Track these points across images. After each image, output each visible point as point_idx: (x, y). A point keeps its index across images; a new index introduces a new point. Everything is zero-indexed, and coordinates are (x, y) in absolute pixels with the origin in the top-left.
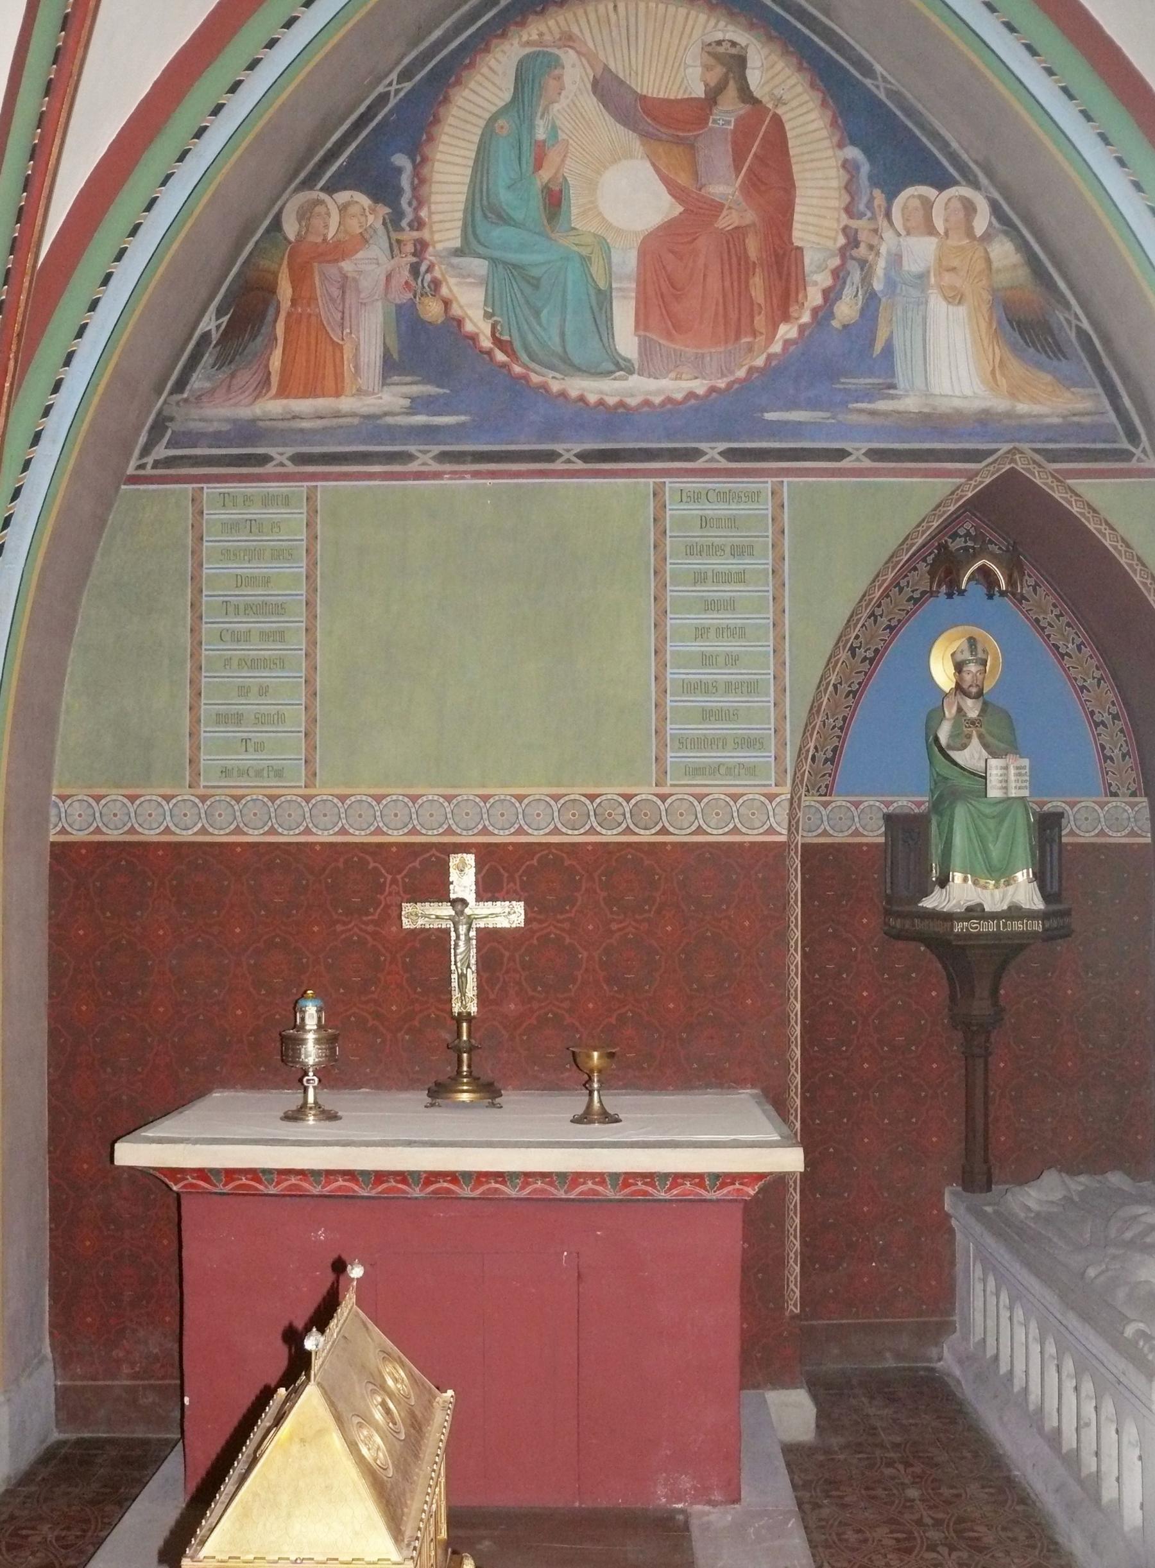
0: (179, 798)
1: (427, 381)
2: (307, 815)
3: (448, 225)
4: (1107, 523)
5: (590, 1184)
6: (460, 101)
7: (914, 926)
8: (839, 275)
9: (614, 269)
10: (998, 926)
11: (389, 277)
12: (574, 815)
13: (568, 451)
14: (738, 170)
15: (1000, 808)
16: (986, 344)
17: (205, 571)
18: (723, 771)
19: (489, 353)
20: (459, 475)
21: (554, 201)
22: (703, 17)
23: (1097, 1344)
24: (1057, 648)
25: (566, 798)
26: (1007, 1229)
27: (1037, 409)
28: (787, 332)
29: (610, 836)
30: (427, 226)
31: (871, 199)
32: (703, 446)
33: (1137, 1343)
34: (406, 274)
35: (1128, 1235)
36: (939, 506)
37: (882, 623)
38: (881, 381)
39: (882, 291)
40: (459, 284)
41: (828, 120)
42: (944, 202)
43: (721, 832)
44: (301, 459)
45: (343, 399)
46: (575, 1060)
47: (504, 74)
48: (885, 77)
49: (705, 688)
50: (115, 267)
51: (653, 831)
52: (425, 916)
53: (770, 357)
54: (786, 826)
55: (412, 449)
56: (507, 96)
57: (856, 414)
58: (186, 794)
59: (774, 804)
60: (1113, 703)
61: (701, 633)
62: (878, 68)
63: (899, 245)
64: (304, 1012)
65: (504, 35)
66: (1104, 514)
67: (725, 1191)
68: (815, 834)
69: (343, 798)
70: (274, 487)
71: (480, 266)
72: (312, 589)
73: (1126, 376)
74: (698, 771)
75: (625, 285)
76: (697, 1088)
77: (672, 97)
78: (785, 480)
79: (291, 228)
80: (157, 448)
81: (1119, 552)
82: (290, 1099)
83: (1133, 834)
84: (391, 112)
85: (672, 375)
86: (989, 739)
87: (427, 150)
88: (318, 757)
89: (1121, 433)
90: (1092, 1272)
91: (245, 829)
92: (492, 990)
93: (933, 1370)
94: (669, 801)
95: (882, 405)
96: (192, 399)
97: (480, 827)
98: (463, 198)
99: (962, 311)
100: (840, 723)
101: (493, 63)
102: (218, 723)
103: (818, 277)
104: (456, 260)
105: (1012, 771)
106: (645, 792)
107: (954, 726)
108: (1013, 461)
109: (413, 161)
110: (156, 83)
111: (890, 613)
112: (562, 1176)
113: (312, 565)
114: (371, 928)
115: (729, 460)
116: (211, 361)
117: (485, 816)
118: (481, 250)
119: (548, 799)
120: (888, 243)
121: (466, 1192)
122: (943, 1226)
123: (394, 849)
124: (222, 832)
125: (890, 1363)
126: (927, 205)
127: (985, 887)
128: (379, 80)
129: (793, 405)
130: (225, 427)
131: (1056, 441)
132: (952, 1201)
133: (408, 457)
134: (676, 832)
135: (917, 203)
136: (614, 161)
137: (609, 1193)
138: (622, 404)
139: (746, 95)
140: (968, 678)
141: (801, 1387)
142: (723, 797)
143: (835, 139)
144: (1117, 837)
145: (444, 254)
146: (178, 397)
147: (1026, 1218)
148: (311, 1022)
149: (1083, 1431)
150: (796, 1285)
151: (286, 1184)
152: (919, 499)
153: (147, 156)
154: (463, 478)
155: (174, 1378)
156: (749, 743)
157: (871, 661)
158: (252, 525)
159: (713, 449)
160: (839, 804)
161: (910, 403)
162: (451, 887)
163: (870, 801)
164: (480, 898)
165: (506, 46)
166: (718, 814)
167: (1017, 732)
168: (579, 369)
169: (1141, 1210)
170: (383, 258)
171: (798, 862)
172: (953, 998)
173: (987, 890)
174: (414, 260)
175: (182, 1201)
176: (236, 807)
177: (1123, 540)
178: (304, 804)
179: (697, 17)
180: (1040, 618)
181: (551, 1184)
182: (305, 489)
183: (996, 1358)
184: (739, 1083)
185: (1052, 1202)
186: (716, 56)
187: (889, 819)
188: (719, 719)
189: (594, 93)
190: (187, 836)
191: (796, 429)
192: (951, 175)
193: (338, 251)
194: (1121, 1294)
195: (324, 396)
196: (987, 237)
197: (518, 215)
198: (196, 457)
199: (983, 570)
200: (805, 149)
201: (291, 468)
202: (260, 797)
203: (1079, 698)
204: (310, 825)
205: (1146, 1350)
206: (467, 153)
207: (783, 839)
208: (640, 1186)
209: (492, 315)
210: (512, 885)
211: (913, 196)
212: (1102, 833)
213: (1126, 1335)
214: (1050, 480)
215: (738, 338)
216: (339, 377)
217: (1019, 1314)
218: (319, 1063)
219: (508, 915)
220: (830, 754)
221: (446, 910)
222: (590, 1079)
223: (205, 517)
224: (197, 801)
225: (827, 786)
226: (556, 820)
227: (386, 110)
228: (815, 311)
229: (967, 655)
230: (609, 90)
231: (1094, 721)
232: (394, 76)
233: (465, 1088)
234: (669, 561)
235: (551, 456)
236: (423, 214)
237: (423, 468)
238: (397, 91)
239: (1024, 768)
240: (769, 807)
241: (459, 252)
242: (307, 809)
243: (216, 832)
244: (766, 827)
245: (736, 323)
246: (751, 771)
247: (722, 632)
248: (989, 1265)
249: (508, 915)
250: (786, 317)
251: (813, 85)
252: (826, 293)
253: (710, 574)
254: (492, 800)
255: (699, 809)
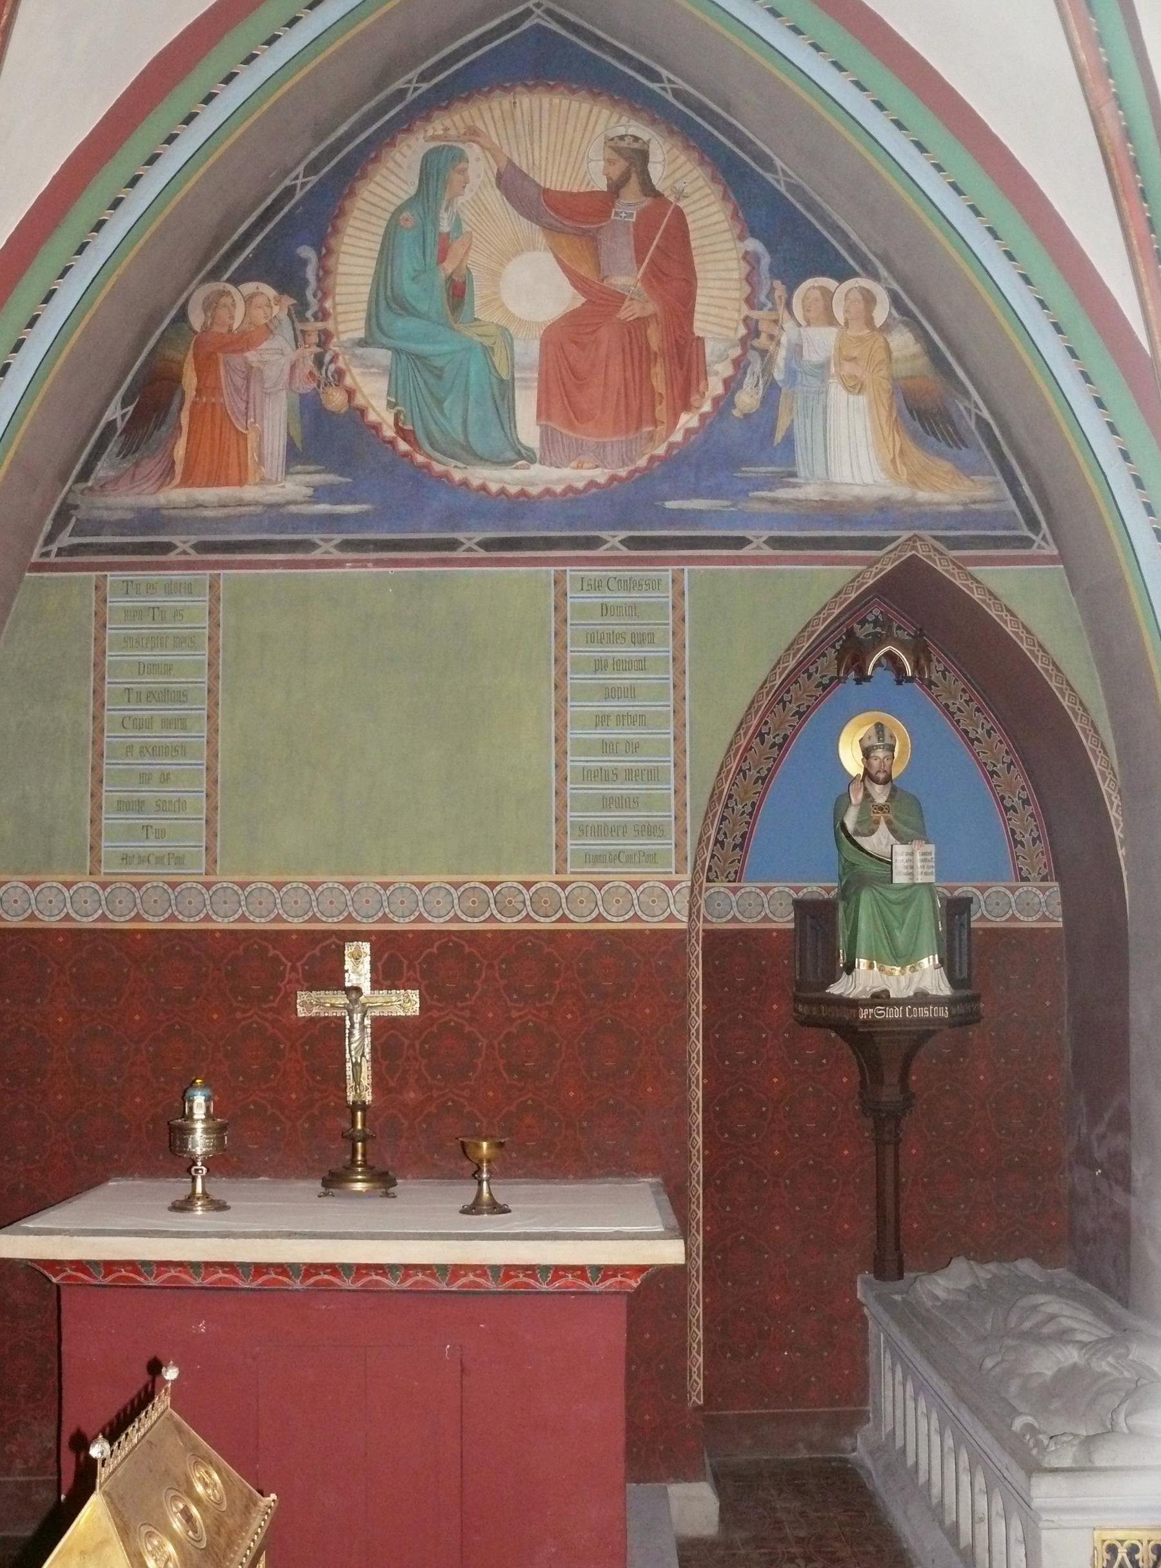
0: (80, 885)
1: (328, 471)
2: (208, 902)
3: (352, 316)
4: (1008, 610)
5: (471, 1277)
6: (365, 194)
7: (820, 1012)
8: (740, 365)
9: (516, 359)
10: (904, 1011)
11: (293, 367)
12: (474, 902)
13: (469, 539)
14: (640, 262)
15: (908, 892)
16: (886, 434)
17: (108, 659)
18: (623, 858)
19: (392, 442)
20: (362, 563)
21: (457, 292)
22: (606, 113)
23: (985, 1439)
24: (966, 732)
25: (467, 886)
26: (910, 1317)
27: (938, 497)
28: (687, 422)
29: (509, 924)
30: (332, 317)
31: (772, 289)
32: (604, 534)
33: (1024, 1436)
34: (310, 363)
35: (1027, 1325)
36: (839, 593)
37: (791, 709)
38: (782, 469)
39: (783, 381)
40: (363, 374)
41: (729, 213)
42: (843, 292)
43: (621, 919)
44: (203, 547)
45: (247, 488)
46: (464, 1152)
47: (409, 167)
48: (785, 173)
49: (605, 775)
50: (13, 358)
51: (553, 919)
52: (319, 1004)
53: (671, 446)
54: (687, 914)
55: (315, 537)
56: (413, 190)
57: (758, 502)
58: (86, 881)
59: (674, 891)
60: (1023, 788)
61: (602, 720)
62: (778, 163)
63: (800, 335)
64: (192, 1101)
65: (409, 130)
66: (1005, 601)
67: (608, 1283)
68: (724, 920)
69: (243, 885)
70: (176, 575)
71: (383, 356)
72: (214, 677)
73: (1024, 463)
74: (597, 859)
75: (528, 375)
76: (596, 1177)
77: (575, 190)
78: (686, 568)
79: (197, 319)
80: (61, 536)
81: (1021, 639)
82: (178, 1188)
83: (1044, 918)
84: (296, 206)
85: (574, 464)
86: (897, 824)
87: (332, 242)
88: (218, 844)
89: (1022, 521)
90: (989, 1363)
91: (145, 916)
92: (392, 1078)
93: (845, 1461)
94: (569, 889)
95: (783, 493)
96: (97, 488)
97: (380, 914)
98: (367, 289)
99: (862, 400)
100: (748, 809)
101: (399, 157)
102: (119, 810)
103: (718, 367)
104: (359, 351)
105: (918, 857)
106: (546, 879)
107: (861, 812)
108: (914, 548)
109: (319, 252)
110: (54, 177)
111: (797, 700)
112: (443, 1268)
113: (214, 652)
114: (270, 1016)
115: (629, 548)
116: (116, 450)
117: (385, 904)
118: (384, 340)
119: (448, 887)
120: (789, 333)
121: (347, 1284)
122: (855, 1315)
123: (294, 937)
124: (122, 919)
125: (803, 1454)
126: (828, 295)
127: (892, 974)
128: (286, 173)
129: (696, 494)
130: (129, 516)
131: (956, 529)
132: (865, 1289)
133: (309, 546)
134: (576, 919)
135: (817, 293)
136: (518, 253)
137: (491, 1285)
138: (523, 493)
139: (648, 188)
140: (875, 763)
141: (705, 1480)
142: (623, 884)
143: (737, 231)
144: (1028, 922)
145: (348, 344)
146: (81, 486)
147: (934, 1306)
148: (199, 1113)
149: (977, 1526)
150: (699, 1376)
151: (166, 1276)
152: (821, 587)
153: (45, 249)
154: (366, 567)
155: (51, 1474)
156: (650, 830)
157: (781, 746)
158: (156, 613)
159: (614, 537)
160: (748, 890)
161: (811, 492)
162: (346, 975)
163: (779, 887)
164: (376, 985)
165: (412, 141)
166: (618, 901)
167: (926, 817)
168: (481, 459)
169: (1041, 1299)
170: (289, 349)
171: (699, 949)
172: (863, 1083)
173: (900, 977)
174: (319, 350)
175: (63, 1295)
176: (137, 895)
177: (1024, 627)
178: (204, 891)
179: (600, 112)
180: (950, 703)
181: (432, 1275)
182: (208, 577)
183: (903, 1450)
184: (639, 1171)
185: (960, 1291)
186: (617, 150)
187: (798, 904)
188: (620, 807)
189: (499, 187)
190: (87, 923)
191: (696, 518)
192: (851, 267)
193: (244, 341)
194: (1014, 1386)
195: (227, 484)
196: (887, 328)
197: (422, 307)
198: (101, 545)
199: (889, 655)
200: (706, 242)
201: (194, 556)
202: (161, 884)
203: (989, 783)
204: (211, 913)
205: (1031, 1444)
206: (372, 245)
207: (684, 926)
208: (522, 1278)
209: (396, 404)
210: (411, 972)
211: (814, 287)
212: (1013, 918)
213: (1014, 1428)
214: (951, 567)
215: (639, 427)
216: (242, 466)
217: (922, 1404)
218: (206, 1153)
219: (406, 1003)
220: (739, 841)
221: (341, 999)
222: (479, 1170)
223: (109, 604)
224: (97, 888)
225: (736, 872)
226: (457, 907)
227: (293, 202)
228: (716, 401)
229: (874, 741)
230: (512, 183)
231: (1005, 807)
232: (300, 169)
233: (359, 1177)
234: (569, 649)
235: (453, 545)
236: (328, 305)
237: (327, 557)
238: (304, 185)
239: (930, 853)
240: (670, 895)
241: (363, 343)
242: (207, 896)
243: (116, 919)
244: (666, 914)
245: (637, 412)
246: (651, 858)
247: (622, 719)
248: (897, 1356)
249: (406, 1003)
250: (687, 407)
251: (714, 179)
252: (727, 382)
253: (610, 662)
254: (392, 888)
255: (599, 897)
